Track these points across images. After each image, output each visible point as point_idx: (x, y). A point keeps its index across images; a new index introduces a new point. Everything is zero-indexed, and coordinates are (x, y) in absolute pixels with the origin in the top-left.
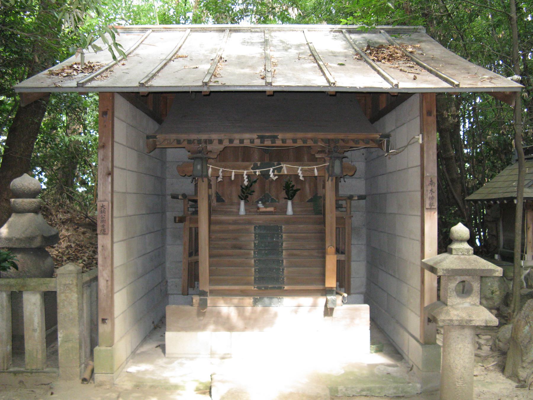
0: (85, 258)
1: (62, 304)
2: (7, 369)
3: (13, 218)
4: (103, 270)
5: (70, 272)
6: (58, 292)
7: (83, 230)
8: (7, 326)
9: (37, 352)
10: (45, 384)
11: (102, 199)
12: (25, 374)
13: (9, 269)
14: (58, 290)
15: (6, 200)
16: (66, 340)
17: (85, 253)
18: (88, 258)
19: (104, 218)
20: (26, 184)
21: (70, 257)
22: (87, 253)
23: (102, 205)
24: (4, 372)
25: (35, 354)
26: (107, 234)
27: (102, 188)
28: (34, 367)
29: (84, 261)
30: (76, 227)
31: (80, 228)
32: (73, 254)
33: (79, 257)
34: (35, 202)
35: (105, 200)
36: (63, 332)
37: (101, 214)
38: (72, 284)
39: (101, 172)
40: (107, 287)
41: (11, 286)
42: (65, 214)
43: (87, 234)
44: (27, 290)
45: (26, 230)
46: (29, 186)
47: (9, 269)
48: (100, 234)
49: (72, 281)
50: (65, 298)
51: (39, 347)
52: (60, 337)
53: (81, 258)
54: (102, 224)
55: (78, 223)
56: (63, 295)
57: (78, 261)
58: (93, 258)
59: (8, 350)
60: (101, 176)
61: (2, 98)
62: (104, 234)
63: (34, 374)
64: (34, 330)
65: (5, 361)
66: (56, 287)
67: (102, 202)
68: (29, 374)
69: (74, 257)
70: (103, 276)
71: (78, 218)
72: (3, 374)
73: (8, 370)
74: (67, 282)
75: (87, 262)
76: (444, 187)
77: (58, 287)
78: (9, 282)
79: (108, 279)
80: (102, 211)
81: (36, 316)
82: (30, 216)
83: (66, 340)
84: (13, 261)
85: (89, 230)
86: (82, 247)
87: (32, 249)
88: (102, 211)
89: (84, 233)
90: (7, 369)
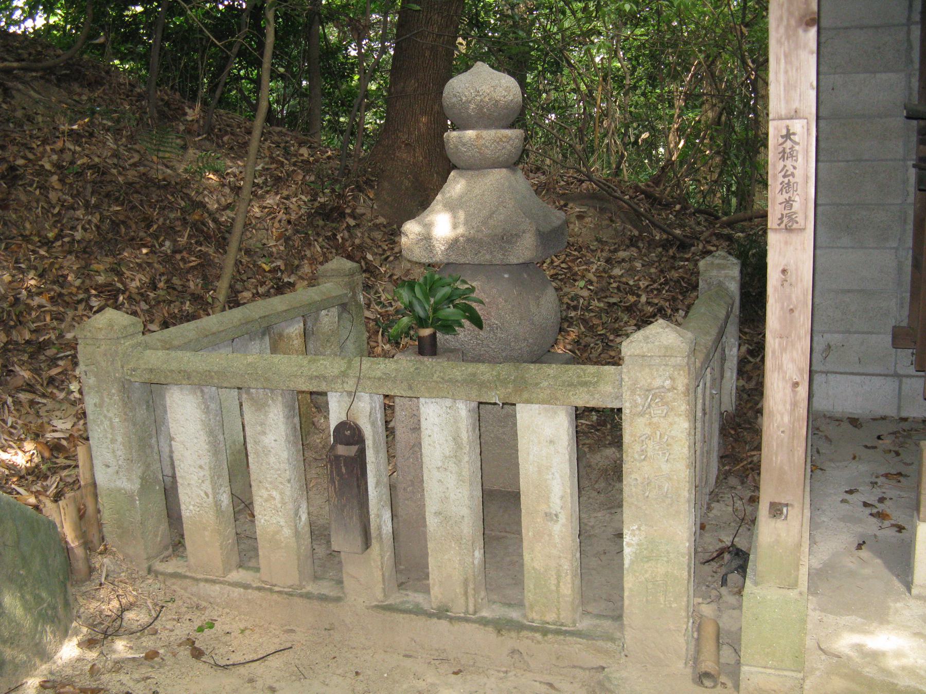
0: (591, 276)
1: (637, 448)
2: (475, 612)
3: (456, 185)
4: (783, 349)
5: (667, 353)
6: (626, 412)
7: (578, 210)
8: (471, 497)
9: (558, 577)
10: (581, 668)
11: (783, 113)
12: (525, 633)
13: (461, 326)
14: (627, 405)
15: (406, 145)
16: (648, 555)
17: (588, 263)
18: (597, 277)
19: (793, 175)
20: (485, 88)
21: (557, 274)
22: (593, 263)
23: (784, 132)
24: (467, 620)
25: (553, 581)
26: (803, 230)
27: (786, 72)
28: (551, 617)
29: (590, 282)
30: (562, 203)
31: (570, 205)
32: (563, 265)
33: (576, 274)
34: (510, 139)
35: (795, 115)
36: (639, 529)
37: (781, 163)
38: (674, 388)
39: (781, 18)
40: (794, 404)
41: (482, 385)
42: (531, 175)
43: (588, 220)
44: (529, 401)
45: (491, 216)
46: (494, 95)
47: (461, 326)
48: (775, 230)
49: (672, 378)
50: (648, 431)
51: (566, 566)
52: (629, 545)
53: (583, 277)
54: (786, 196)
55: (564, 194)
56: (641, 421)
57: (576, 284)
58: (610, 277)
59: (476, 562)
60: (782, 30)
61: (33, 682)
62: (789, 230)
63: (550, 636)
64: (551, 517)
65: (471, 592)
66: (619, 397)
67: (788, 122)
68: (538, 636)
69: (565, 274)
70: (780, 367)
71: (562, 183)
72: (466, 625)
73: (477, 615)
74: (658, 382)
75: (595, 284)
76: (526, 166)
77: (626, 395)
78: (474, 375)
79: (796, 378)
80: (784, 151)
81: (557, 475)
82: (498, 176)
83: (648, 555)
84: (469, 303)
85: (591, 212)
86: (579, 249)
87: (507, 267)
88: (784, 151)
89: (580, 217)
90: (475, 612)
